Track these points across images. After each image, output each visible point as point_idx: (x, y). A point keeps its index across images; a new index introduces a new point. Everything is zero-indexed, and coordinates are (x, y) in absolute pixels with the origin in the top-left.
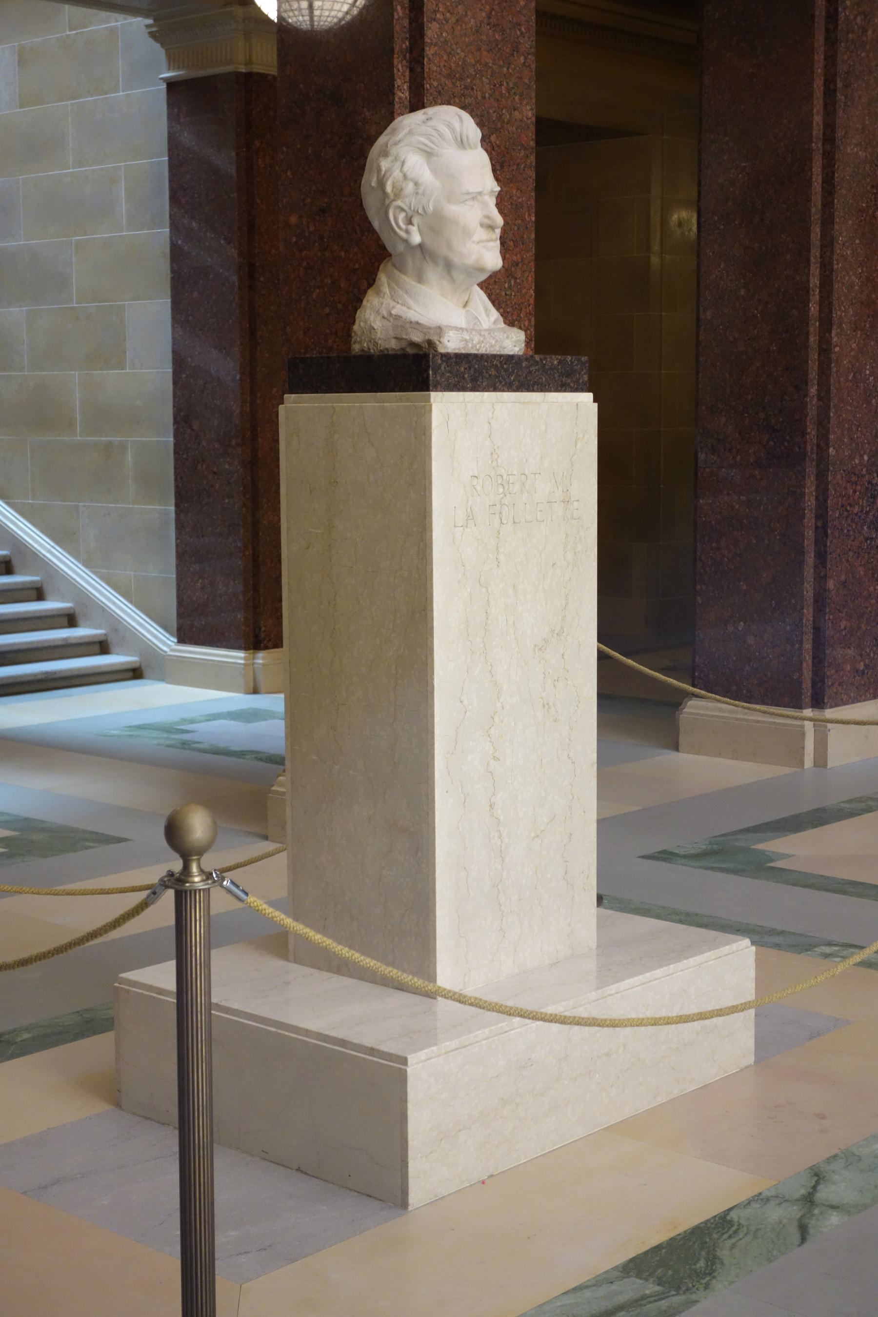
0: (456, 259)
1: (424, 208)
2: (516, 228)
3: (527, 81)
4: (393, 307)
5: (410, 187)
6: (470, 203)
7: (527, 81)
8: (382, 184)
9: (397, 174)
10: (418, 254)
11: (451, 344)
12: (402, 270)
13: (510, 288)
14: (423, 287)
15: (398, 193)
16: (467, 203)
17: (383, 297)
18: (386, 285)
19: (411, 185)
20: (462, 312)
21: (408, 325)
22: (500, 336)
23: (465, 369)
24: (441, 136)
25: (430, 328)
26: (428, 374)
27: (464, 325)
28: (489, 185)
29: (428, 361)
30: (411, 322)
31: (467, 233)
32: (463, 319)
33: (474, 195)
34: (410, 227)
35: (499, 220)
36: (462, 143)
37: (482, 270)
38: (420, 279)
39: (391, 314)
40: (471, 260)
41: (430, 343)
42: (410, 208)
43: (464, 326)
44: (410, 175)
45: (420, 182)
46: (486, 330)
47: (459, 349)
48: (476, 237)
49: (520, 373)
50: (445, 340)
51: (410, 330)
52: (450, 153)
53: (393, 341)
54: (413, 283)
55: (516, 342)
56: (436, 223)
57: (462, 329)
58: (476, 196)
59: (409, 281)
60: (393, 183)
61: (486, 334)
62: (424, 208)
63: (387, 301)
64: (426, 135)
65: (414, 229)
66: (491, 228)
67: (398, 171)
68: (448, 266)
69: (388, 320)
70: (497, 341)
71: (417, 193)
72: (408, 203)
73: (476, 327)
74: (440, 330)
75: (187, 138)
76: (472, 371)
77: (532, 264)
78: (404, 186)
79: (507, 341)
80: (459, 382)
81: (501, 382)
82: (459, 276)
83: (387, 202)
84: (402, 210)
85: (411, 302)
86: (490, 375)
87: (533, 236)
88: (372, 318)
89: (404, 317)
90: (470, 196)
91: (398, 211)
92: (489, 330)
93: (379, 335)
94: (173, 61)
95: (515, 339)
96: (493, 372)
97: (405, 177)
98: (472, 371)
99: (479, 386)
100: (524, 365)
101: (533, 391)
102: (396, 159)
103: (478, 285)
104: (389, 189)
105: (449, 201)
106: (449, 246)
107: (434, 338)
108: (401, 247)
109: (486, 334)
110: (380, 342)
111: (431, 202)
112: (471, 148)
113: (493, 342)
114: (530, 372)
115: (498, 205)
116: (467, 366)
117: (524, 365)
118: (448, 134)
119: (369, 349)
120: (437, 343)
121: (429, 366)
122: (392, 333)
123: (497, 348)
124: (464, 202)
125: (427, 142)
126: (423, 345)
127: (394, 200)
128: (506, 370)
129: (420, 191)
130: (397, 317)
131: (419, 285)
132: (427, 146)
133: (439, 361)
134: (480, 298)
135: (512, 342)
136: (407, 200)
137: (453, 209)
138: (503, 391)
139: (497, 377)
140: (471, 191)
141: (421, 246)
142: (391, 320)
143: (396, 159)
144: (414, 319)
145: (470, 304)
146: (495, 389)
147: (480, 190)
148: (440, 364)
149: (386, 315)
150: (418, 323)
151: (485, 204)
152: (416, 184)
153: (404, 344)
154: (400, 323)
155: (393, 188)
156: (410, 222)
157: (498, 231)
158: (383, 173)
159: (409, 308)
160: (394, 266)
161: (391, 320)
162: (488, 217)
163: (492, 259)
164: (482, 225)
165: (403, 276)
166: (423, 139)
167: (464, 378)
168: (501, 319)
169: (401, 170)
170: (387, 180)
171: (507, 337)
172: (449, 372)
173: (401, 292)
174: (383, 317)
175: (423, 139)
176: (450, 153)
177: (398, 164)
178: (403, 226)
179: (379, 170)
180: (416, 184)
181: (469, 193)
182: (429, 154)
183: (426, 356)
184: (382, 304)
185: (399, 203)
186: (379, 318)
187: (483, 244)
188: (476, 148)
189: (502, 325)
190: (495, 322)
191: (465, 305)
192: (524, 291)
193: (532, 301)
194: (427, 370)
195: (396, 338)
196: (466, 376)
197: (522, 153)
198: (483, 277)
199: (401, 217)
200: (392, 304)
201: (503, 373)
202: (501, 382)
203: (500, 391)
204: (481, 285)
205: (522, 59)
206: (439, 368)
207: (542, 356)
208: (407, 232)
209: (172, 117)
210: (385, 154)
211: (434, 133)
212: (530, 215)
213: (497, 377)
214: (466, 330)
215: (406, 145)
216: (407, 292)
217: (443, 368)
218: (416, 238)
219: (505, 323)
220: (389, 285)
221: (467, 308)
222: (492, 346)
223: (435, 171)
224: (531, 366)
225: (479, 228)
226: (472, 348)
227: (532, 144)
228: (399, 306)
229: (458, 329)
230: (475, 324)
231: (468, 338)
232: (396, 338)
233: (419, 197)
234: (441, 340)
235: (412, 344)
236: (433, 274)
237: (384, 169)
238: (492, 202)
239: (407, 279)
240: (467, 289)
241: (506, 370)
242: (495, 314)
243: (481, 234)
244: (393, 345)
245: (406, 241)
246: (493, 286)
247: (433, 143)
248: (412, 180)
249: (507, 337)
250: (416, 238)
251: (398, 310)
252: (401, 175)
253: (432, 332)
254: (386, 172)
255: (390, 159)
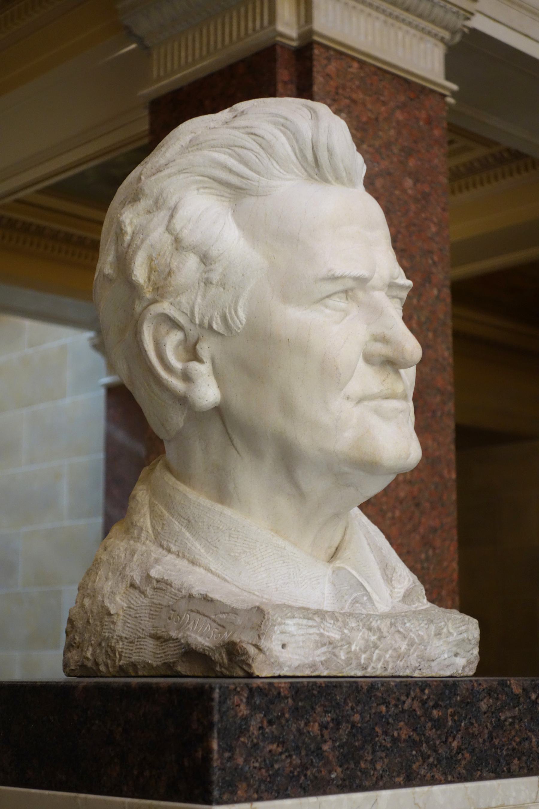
0: (304, 440)
1: (224, 319)
2: (433, 487)
3: (441, 316)
4: (157, 561)
5: (189, 267)
6: (339, 303)
7: (441, 316)
8: (124, 263)
9: (158, 235)
10: (215, 432)
11: (290, 652)
12: (182, 475)
13: (427, 559)
14: (227, 511)
15: (162, 282)
16: (330, 302)
17: (138, 539)
18: (146, 510)
19: (192, 262)
20: (324, 571)
21: (183, 605)
22: (418, 629)
23: (323, 726)
24: (267, 147)
25: (235, 611)
26: (209, 751)
27: (328, 604)
28: (382, 263)
29: (209, 711)
30: (191, 596)
31: (330, 375)
32: (327, 588)
33: (350, 284)
34: (195, 366)
35: (412, 347)
36: (316, 167)
37: (369, 466)
38: (222, 493)
39: (148, 578)
40: (343, 442)
41: (233, 650)
42: (192, 320)
43: (328, 605)
44: (189, 236)
45: (214, 252)
46: (383, 617)
47: (313, 666)
48: (354, 387)
49: (475, 730)
50: (272, 644)
51: (187, 617)
52: (290, 191)
53: (150, 644)
54: (205, 501)
55: (459, 643)
56: (256, 354)
57: (321, 614)
58: (353, 288)
59: (195, 498)
60: (151, 259)
61: (384, 625)
62: (224, 319)
63: (146, 547)
64: (230, 147)
65: (202, 370)
66: (392, 364)
67: (161, 229)
68: (288, 459)
69: (143, 593)
70: (411, 644)
71: (208, 282)
72: (186, 307)
73: (359, 609)
74: (259, 617)
75: (121, 436)
76: (345, 728)
77: (454, 532)
78: (174, 265)
79: (436, 642)
80: (304, 767)
81: (425, 758)
82: (315, 485)
83: (138, 308)
84: (175, 325)
85: (198, 548)
86: (395, 740)
87: (454, 497)
88: (107, 587)
89: (177, 583)
90: (338, 286)
91: (163, 329)
92: (393, 617)
93: (120, 629)
94: (111, 368)
95: (455, 637)
96: (404, 731)
97: (178, 242)
98: (345, 728)
99: (365, 772)
100: (483, 706)
101: (510, 774)
102: (157, 205)
103: (361, 507)
104: (140, 273)
105: (286, 298)
106: (288, 407)
107: (244, 639)
108: (178, 419)
109: (384, 625)
110: (119, 646)
111: (241, 303)
112: (338, 179)
113: (404, 647)
114: (500, 725)
115: (407, 319)
116: (328, 718)
117: (483, 706)
118: (283, 144)
119: (97, 664)
120: (252, 650)
121: (211, 725)
122: (147, 625)
123: (413, 661)
124: (322, 300)
125: (232, 162)
126: (216, 657)
127: (154, 301)
128: (438, 724)
129: (215, 277)
130: (162, 585)
131: (219, 507)
132: (231, 171)
133: (244, 710)
134: (369, 543)
135: (448, 645)
136: (183, 299)
137: (293, 317)
138: (433, 782)
139: (414, 744)
140: (338, 272)
141: (219, 411)
142: (149, 591)
143: (158, 204)
144: (198, 589)
145: (346, 554)
146: (411, 780)
147: (361, 271)
148: (246, 719)
149: (138, 582)
150: (206, 599)
151: (375, 312)
152: (205, 259)
153: (171, 653)
154: (166, 600)
155: (151, 269)
156: (193, 355)
157: (409, 375)
158: (128, 238)
159: (193, 562)
160: (168, 468)
161: (149, 591)
162: (384, 340)
163: (395, 440)
164: (368, 359)
165: (182, 487)
166: (223, 157)
167: (319, 752)
168: (421, 589)
169: (169, 229)
170: (135, 252)
171: (438, 634)
172: (275, 739)
173: (176, 525)
174: (132, 586)
175: (223, 157)
176: (290, 191)
177: (163, 215)
178: (177, 365)
179: (120, 232)
180: (205, 259)
181: (334, 278)
182: (235, 191)
183: (202, 694)
184: (133, 553)
185: (165, 307)
186: (122, 587)
187: (373, 404)
188: (352, 183)
189: (424, 604)
190: (407, 597)
191: (333, 556)
192: (445, 564)
193: (455, 576)
194: (203, 738)
195: (156, 637)
196: (326, 747)
197: (438, 399)
198: (374, 487)
199: (172, 341)
200: (156, 552)
201: (431, 733)
202: (425, 758)
203: (423, 782)
204: (372, 508)
205: (435, 292)
206: (243, 730)
207: (527, 681)
208: (187, 377)
209: (110, 418)
210: (135, 197)
211: (249, 142)
212: (449, 472)
213: (414, 744)
214: (333, 615)
215: (180, 172)
216: (189, 524)
217: (254, 729)
218: (208, 393)
219: (431, 600)
220: (152, 511)
221: (338, 563)
222: (400, 657)
223: (250, 228)
224: (501, 709)
225: (361, 364)
226: (348, 662)
227: (450, 388)
228: (170, 558)
229: (306, 612)
230: (356, 601)
231: (335, 635)
232: (156, 637)
233: (213, 290)
234: (263, 643)
235: (191, 654)
236: (251, 478)
237: (129, 230)
238: (394, 312)
239: (192, 494)
240: (337, 515)
241: (438, 724)
242: (405, 578)
243: (366, 379)
244: (149, 653)
245: (183, 401)
246: (395, 510)
247: (246, 164)
248: (194, 249)
249: (438, 634)
250: (208, 393)
251: (168, 567)
252: (168, 239)
253: (239, 621)
254: (134, 234)
255: (143, 204)
